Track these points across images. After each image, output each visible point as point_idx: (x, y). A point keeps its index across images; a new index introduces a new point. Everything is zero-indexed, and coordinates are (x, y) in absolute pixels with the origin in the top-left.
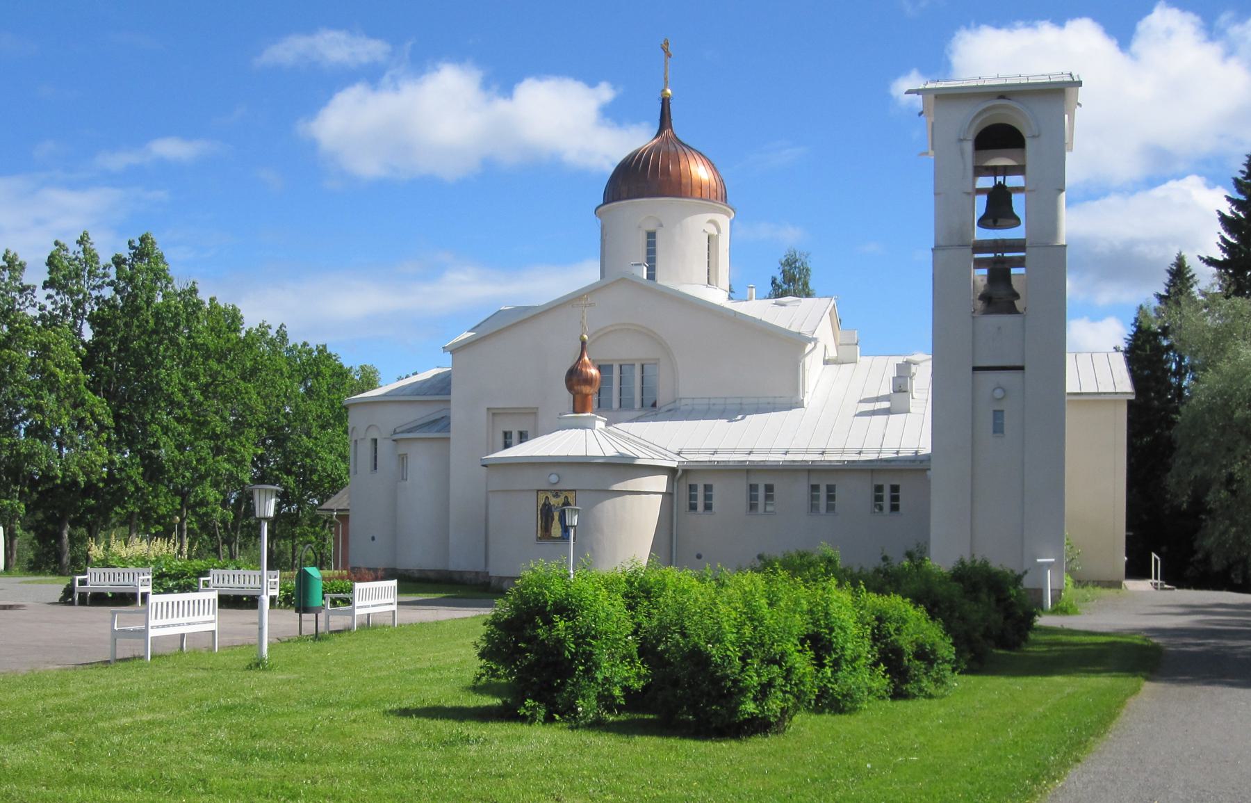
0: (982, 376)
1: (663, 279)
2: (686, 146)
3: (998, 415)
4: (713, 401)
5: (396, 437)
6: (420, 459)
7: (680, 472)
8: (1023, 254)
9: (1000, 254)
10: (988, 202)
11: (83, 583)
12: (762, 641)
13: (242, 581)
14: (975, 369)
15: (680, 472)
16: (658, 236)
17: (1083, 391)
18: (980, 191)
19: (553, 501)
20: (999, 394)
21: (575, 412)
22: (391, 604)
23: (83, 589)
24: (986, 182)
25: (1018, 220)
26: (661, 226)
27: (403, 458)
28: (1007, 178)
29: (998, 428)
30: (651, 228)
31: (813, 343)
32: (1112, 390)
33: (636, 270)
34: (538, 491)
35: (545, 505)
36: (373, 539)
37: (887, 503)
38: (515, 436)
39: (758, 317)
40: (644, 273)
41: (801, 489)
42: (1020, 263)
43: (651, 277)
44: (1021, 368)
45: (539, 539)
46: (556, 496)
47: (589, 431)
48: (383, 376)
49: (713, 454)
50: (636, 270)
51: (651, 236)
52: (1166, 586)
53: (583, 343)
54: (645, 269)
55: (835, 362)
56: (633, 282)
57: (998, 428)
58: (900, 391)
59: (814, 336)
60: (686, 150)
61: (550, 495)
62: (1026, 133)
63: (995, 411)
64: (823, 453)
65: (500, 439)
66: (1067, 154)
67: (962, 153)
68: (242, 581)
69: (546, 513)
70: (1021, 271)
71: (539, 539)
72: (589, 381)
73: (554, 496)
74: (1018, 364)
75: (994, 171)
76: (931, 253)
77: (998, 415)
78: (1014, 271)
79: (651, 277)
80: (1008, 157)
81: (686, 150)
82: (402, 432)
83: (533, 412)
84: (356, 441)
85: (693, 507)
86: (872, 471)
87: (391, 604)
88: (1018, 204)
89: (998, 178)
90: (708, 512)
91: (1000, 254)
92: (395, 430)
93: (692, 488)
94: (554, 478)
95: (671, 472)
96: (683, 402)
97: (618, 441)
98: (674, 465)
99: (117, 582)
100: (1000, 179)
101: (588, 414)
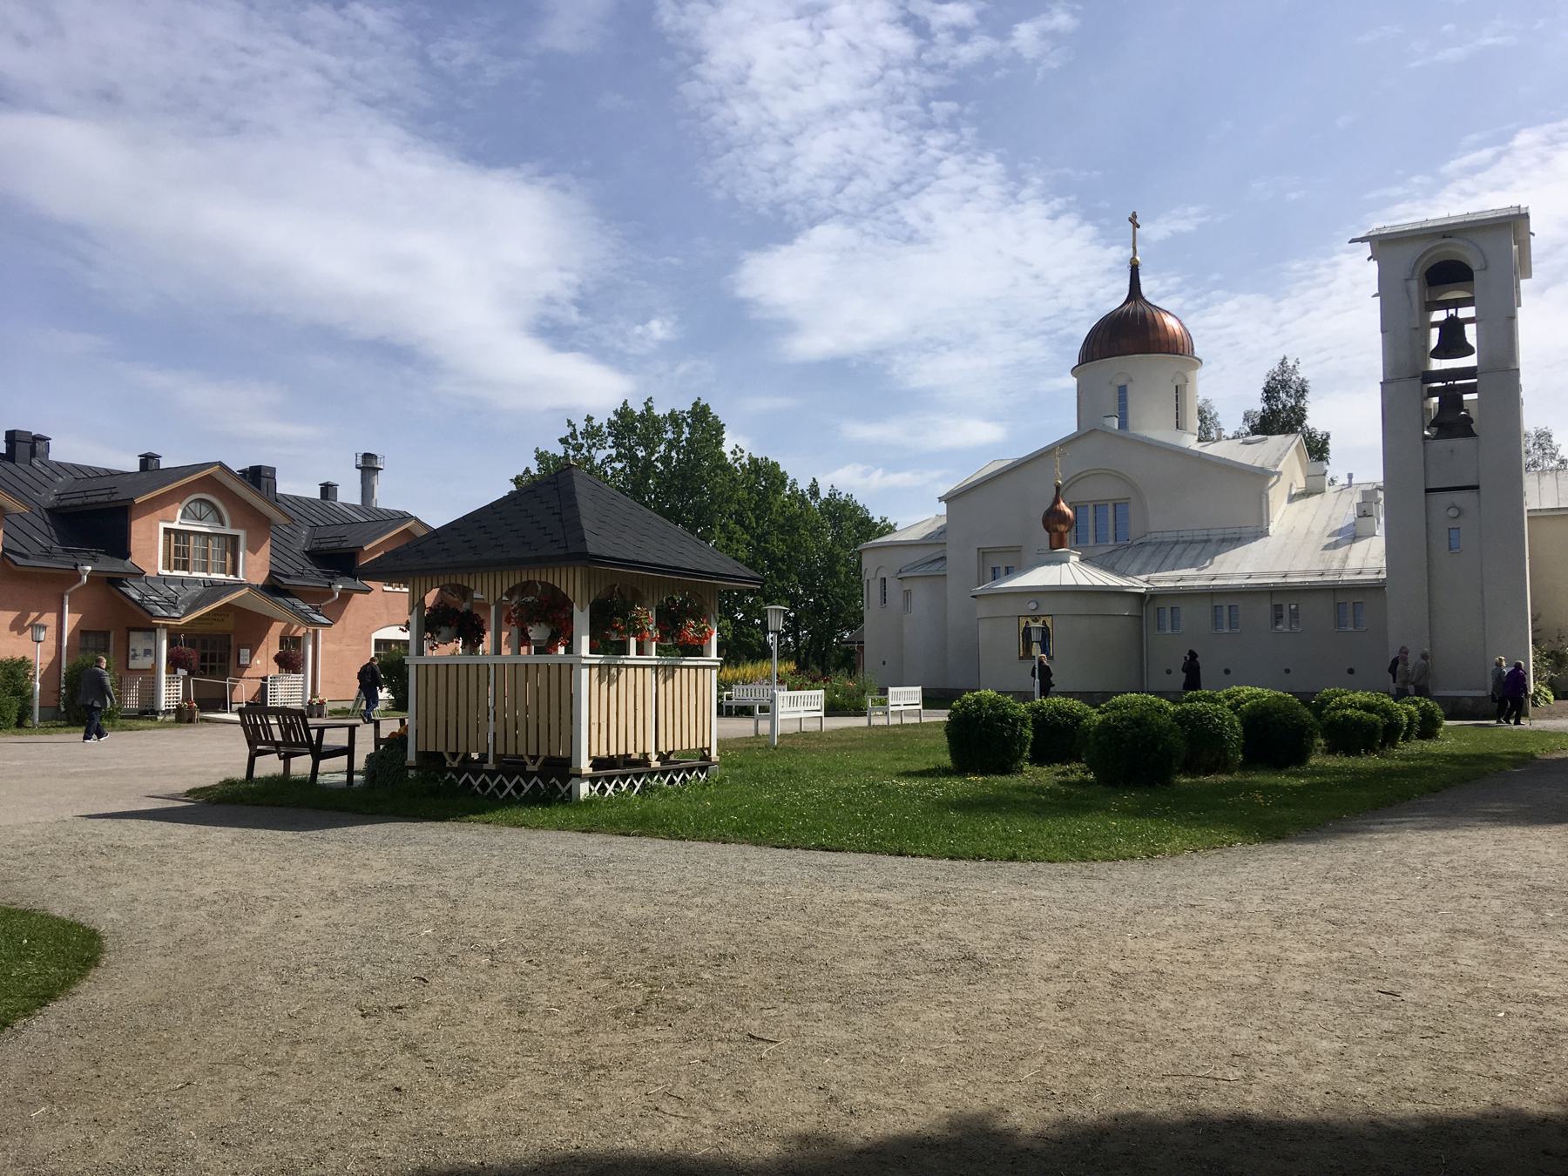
0: (1435, 497)
2: (1150, 304)
4: (1181, 534)
5: (900, 576)
6: (921, 594)
8: (1475, 380)
9: (1452, 382)
10: (1440, 334)
11: (729, 698)
12: (370, 721)
13: (757, 694)
14: (1428, 491)
16: (1129, 388)
17: (1561, 506)
18: (1435, 325)
19: (1033, 625)
20: (1452, 513)
22: (819, 711)
23: (729, 703)
24: (1439, 316)
25: (1473, 348)
26: (1131, 380)
27: (907, 593)
28: (1459, 309)
30: (1122, 383)
31: (1276, 477)
32: (1538, 507)
33: (1108, 422)
36: (884, 663)
38: (1003, 570)
39: (1223, 456)
40: (1115, 423)
41: (1265, 607)
42: (1471, 389)
43: (1123, 425)
44: (1477, 487)
46: (1036, 621)
47: (1064, 565)
48: (250, 556)
49: (1213, 580)
50: (1108, 422)
51: (1122, 391)
53: (1058, 488)
54: (1116, 420)
55: (1307, 494)
56: (1106, 432)
58: (1365, 516)
59: (1277, 470)
60: (1153, 309)
61: (1029, 620)
62: (1475, 265)
64: (1378, 573)
65: (989, 574)
66: (1524, 283)
67: (1408, 291)
68: (757, 694)
70: (1474, 396)
72: (1063, 517)
73: (1033, 621)
74: (1474, 483)
75: (1445, 305)
76: (1380, 386)
78: (1466, 397)
79: (1123, 425)
80: (1464, 290)
81: (1153, 309)
82: (906, 571)
83: (1017, 550)
84: (868, 581)
86: (1334, 590)
87: (819, 711)
88: (1471, 333)
89: (1450, 310)
91: (1452, 382)
92: (900, 570)
94: (1033, 606)
96: (1154, 535)
97: (1089, 571)
99: (757, 697)
100: (1452, 311)
101: (1063, 550)
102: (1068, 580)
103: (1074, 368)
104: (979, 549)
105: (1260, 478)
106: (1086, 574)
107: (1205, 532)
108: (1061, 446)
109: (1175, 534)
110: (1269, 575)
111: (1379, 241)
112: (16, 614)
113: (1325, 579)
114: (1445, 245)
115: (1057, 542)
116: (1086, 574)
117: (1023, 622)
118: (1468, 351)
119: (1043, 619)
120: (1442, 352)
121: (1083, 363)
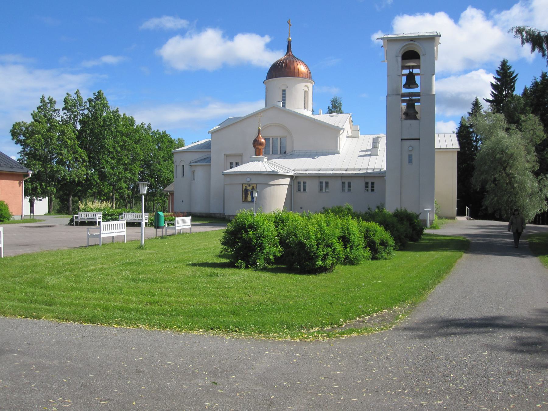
1: (288, 107)
2: (296, 58)
3: (410, 156)
6: (200, 172)
7: (294, 177)
8: (419, 98)
13: (137, 217)
14: (402, 140)
15: (294, 177)
16: (287, 91)
18: (404, 75)
20: (410, 149)
21: (256, 155)
24: (406, 72)
26: (288, 87)
27: (193, 172)
29: (410, 161)
30: (284, 88)
31: (343, 130)
33: (278, 104)
34: (243, 184)
35: (245, 189)
37: (370, 188)
38: (234, 164)
42: (418, 101)
44: (419, 139)
45: (243, 201)
46: (249, 186)
48: (186, 142)
50: (278, 104)
51: (284, 91)
52: (471, 219)
53: (259, 130)
54: (282, 103)
57: (410, 161)
61: (247, 185)
62: (420, 54)
63: (409, 155)
65: (229, 165)
67: (397, 61)
68: (137, 217)
69: (246, 192)
70: (419, 104)
71: (243, 201)
72: (261, 144)
74: (418, 138)
75: (409, 67)
77: (410, 156)
78: (416, 104)
82: (193, 163)
83: (241, 155)
84: (176, 166)
85: (299, 190)
90: (305, 192)
93: (299, 183)
94: (248, 179)
95: (291, 177)
98: (292, 174)
100: (411, 70)
102: (263, 169)
103: (264, 81)
104: (225, 154)
105: (336, 131)
106: (270, 166)
107: (316, 151)
108: (261, 112)
109: (304, 151)
110: (314, 170)
111: (388, 41)
112: (29, 197)
113: (348, 172)
114: (412, 44)
115: (258, 153)
116: (270, 166)
117: (244, 186)
118: (417, 86)
119: (253, 185)
120: (407, 85)
121: (268, 79)
